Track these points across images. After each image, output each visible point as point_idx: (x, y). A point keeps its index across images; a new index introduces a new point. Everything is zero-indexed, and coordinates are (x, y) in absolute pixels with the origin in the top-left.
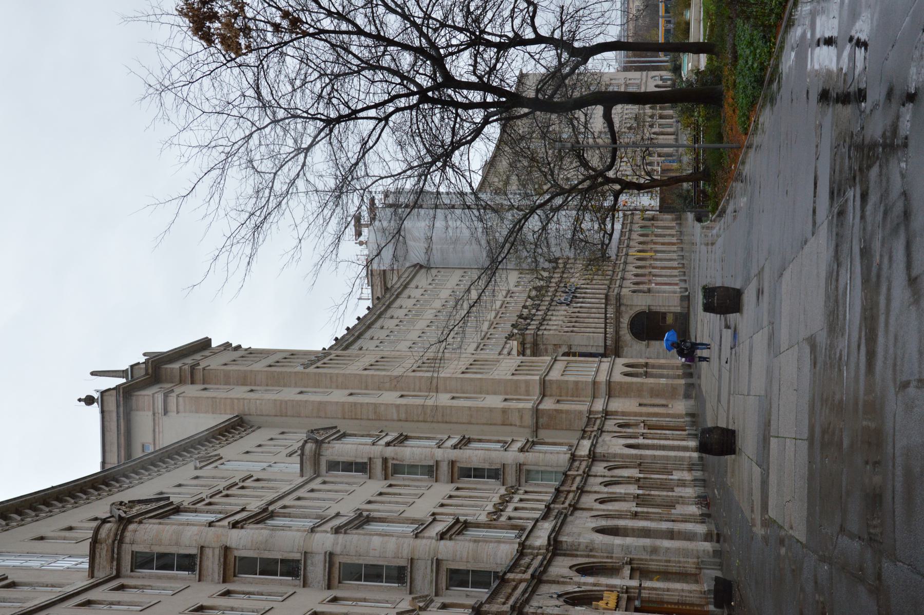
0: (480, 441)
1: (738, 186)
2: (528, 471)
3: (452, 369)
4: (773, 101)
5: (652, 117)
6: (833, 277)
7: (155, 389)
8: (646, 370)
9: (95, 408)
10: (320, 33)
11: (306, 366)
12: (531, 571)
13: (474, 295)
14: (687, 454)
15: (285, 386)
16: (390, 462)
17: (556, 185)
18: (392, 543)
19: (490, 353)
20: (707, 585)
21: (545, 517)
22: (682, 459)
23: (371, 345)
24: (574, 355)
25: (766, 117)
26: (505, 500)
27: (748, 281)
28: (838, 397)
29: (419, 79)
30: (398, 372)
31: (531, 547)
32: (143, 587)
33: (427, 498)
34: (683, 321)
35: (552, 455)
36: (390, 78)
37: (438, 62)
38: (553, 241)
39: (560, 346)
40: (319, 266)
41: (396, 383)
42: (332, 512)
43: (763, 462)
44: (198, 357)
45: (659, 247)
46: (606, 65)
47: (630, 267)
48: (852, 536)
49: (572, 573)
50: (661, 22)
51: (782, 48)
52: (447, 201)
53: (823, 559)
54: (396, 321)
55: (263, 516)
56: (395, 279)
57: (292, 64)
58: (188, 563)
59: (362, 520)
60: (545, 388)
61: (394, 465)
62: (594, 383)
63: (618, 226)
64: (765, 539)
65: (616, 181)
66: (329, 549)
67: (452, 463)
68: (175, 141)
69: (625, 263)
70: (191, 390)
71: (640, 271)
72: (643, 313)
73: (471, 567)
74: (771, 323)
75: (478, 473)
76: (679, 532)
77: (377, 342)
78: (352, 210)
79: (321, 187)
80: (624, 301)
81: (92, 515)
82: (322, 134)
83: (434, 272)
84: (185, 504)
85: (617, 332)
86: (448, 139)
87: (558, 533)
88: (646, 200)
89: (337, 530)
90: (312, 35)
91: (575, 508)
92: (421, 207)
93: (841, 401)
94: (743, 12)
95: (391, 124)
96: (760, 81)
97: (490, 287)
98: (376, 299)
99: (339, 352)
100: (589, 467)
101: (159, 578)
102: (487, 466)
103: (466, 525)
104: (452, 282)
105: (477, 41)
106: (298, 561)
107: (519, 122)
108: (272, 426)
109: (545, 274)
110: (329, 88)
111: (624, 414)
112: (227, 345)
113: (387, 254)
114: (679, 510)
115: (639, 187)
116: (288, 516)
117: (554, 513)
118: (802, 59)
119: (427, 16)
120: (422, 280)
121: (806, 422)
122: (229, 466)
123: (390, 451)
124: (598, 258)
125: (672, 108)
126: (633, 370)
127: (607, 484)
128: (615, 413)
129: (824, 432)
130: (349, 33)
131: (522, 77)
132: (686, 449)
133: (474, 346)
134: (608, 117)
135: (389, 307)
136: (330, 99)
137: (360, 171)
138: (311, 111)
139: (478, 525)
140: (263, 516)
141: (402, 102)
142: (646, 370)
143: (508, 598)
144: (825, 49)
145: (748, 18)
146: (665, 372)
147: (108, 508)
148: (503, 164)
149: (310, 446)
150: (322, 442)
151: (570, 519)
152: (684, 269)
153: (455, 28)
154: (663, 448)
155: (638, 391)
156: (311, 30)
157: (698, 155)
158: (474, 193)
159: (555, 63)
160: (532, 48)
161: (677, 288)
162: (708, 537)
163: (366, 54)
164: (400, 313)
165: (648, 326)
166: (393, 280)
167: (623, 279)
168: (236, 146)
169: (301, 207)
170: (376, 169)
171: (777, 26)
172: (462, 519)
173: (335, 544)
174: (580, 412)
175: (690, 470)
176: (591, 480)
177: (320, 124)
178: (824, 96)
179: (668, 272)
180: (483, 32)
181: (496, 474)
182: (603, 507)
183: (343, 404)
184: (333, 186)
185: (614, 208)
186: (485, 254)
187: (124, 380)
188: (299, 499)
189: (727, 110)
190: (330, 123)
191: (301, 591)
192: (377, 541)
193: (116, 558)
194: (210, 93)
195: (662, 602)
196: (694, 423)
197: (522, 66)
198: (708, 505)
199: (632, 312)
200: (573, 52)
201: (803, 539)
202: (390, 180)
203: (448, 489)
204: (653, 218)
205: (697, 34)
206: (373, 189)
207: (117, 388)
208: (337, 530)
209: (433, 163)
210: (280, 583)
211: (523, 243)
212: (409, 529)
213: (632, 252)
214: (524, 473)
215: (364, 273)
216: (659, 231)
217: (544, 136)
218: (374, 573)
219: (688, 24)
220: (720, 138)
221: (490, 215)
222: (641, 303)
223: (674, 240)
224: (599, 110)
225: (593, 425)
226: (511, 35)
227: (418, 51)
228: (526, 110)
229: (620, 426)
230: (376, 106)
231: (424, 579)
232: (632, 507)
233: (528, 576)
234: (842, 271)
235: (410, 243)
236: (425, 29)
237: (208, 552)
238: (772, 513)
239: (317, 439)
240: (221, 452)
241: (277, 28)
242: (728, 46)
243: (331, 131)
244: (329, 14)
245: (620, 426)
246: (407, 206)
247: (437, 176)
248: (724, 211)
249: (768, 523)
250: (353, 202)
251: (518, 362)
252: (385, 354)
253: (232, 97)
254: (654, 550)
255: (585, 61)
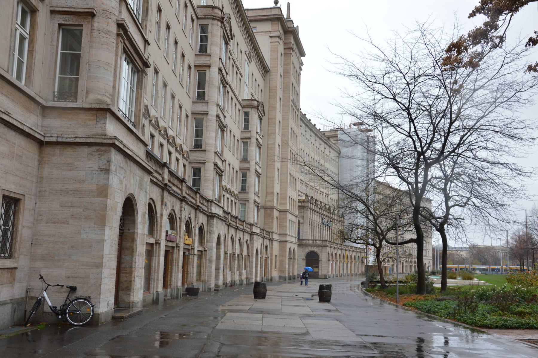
0: (259, 182)
1: (378, 301)
2: (245, 204)
3: (292, 169)
4: (419, 317)
5: (411, 262)
6: (337, 343)
7: (282, 31)
8: (292, 258)
9: (273, 5)
10: (450, 104)
11: (292, 101)
12: (200, 205)
13: (326, 179)
14: (254, 277)
15: (283, 91)
16: (248, 140)
17: (379, 217)
18: (212, 141)
19: (299, 186)
20: (196, 285)
21: (224, 212)
22: (252, 275)
23: (303, 131)
24: (299, 225)
25: (411, 314)
26: (231, 193)
27: (334, 305)
28: (282, 344)
29: (429, 152)
30: (290, 143)
31: (211, 205)
32: (193, 30)
33: (232, 158)
34: (315, 276)
35: (253, 215)
36: (430, 138)
37: (437, 161)
38: (352, 215)
39: (303, 219)
40: (340, 106)
41: (285, 143)
42: (226, 114)
43: (251, 311)
44: (297, 51)
45: (349, 265)
46: (435, 240)
47: (340, 251)
48: (220, 348)
49: (200, 224)
50: (456, 266)
51: (444, 322)
52: (370, 166)
53: (209, 336)
54: (314, 142)
55: (224, 83)
56: (334, 142)
57: (435, 92)
58: (203, 49)
59: (222, 128)
60: (283, 212)
61: (247, 143)
62: (286, 235)
63: (359, 246)
64: (216, 311)
65: (381, 245)
66: (209, 113)
67: (248, 169)
68: (398, 37)
69: (342, 249)
70: (281, 48)
71: (338, 256)
72: (318, 257)
73: (202, 178)
74: (315, 316)
75: (244, 181)
76: (219, 273)
77: (304, 133)
78: (366, 121)
79: (377, 106)
80: (324, 249)
81: (225, 6)
82: (402, 106)
83: (337, 160)
84: (229, 47)
85: (310, 245)
86: (401, 165)
87: (218, 218)
88: (371, 259)
89: (218, 116)
90: (449, 100)
91: (229, 225)
92: (368, 153)
93: (279, 345)
94: (462, 304)
95: (407, 138)
96: (428, 311)
97: (330, 186)
98: (324, 133)
99: (299, 116)
100: (247, 232)
101: (197, 37)
102: (247, 185)
103: (221, 176)
104: (332, 168)
105: (447, 179)
106: (204, 99)
107: (408, 199)
108: (265, 86)
109: (336, 212)
110: (424, 109)
111: (272, 248)
112: (302, 64)
113: (345, 137)
114: (229, 273)
115: (378, 256)
116: (224, 92)
117: (227, 216)
118: (438, 330)
119: (459, 155)
120: (333, 154)
121: (270, 330)
122: (247, 66)
123: (254, 140)
124: (344, 236)
125: (415, 271)
126: (292, 252)
127: (240, 240)
128: (272, 245)
129: (266, 338)
130: (451, 118)
131: (429, 201)
132: (256, 276)
133: (303, 179)
134: (411, 241)
135: (321, 139)
136: (419, 109)
137: (385, 124)
138: (413, 101)
139: (220, 181)
140: (224, 83)
141: (418, 144)
142: (292, 258)
143: (188, 195)
144: (443, 340)
145: (458, 306)
146: (291, 267)
147: (228, 13)
148: (388, 192)
149: (256, 103)
150: (258, 109)
151: (224, 223)
152: (339, 277)
153: (453, 169)
154: (256, 266)
155: (282, 255)
156: (452, 100)
157: (393, 283)
158: (374, 178)
159: (437, 216)
160: (444, 205)
161: (330, 273)
162: (217, 286)
163: (441, 126)
164: (317, 144)
165: (312, 259)
166: (333, 141)
167: (334, 248)
168: (396, 66)
169: (368, 97)
170: (386, 132)
171: (455, 319)
172: (223, 174)
173: (212, 116)
174: (272, 228)
175: (247, 278)
176: (241, 233)
177: (407, 106)
178: (421, 340)
179: (338, 269)
180: (451, 181)
181: (244, 189)
182: (230, 238)
183: (275, 118)
184: (378, 112)
185: (368, 244)
186: (346, 183)
187: (285, 17)
188: (232, 99)
189: (415, 296)
190: (408, 109)
191: (191, 101)
192: (213, 135)
193: (206, 17)
194: (421, 53)
195: (188, 264)
196: (268, 280)
197: (435, 202)
198: (231, 286)
199: (319, 252)
200: (442, 225)
201: (217, 327)
202: (380, 138)
203: (237, 168)
204: (363, 262)
205: (450, 283)
206: (376, 130)
207: (282, 14)
208: (218, 116)
209: (389, 159)
210: (194, 91)
211: (351, 202)
212: (219, 150)
213: (347, 252)
214: (244, 202)
215: (337, 127)
216: (357, 265)
217: (402, 211)
218: (199, 134)
219: (455, 278)
220: (401, 293)
221: (365, 186)
222: (323, 256)
223: (353, 272)
224: (414, 237)
225: (266, 234)
226: (450, 195)
227: (442, 151)
228: (414, 202)
229: (266, 247)
230: (416, 131)
231: (196, 156)
232: (230, 252)
233: (198, 204)
234: (340, 348)
235: (350, 149)
236: (453, 154)
237: (208, 58)
238: (228, 314)
239: (259, 107)
240: (253, 63)
241: (455, 82)
242: (445, 297)
243: (404, 110)
244: (460, 109)
245: (266, 247)
246: (368, 147)
247: (382, 160)
248: (366, 294)
249: (224, 312)
250: (370, 121)
251: (295, 199)
252: (299, 137)
253: (419, 63)
254: (211, 261)
255: (438, 230)
